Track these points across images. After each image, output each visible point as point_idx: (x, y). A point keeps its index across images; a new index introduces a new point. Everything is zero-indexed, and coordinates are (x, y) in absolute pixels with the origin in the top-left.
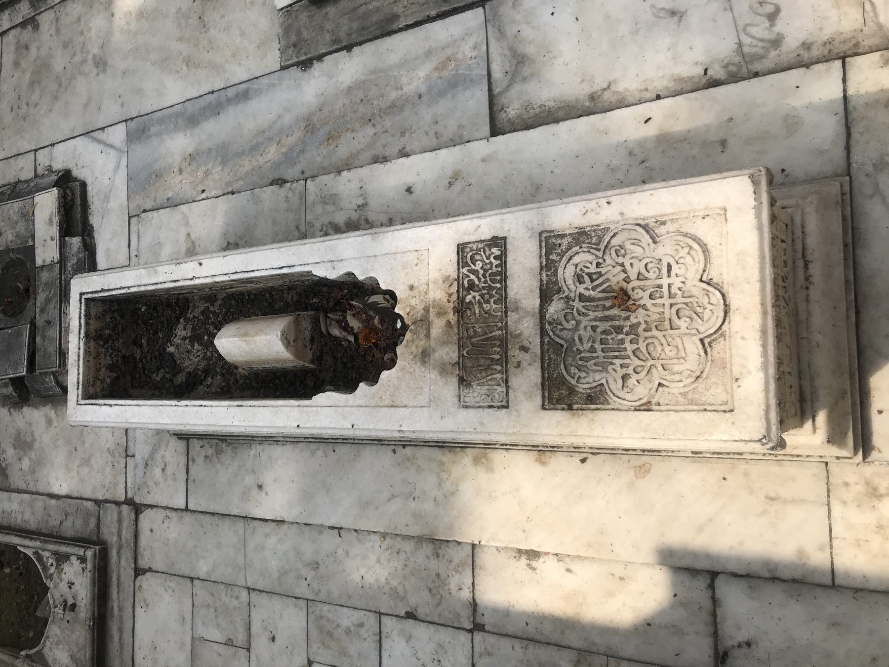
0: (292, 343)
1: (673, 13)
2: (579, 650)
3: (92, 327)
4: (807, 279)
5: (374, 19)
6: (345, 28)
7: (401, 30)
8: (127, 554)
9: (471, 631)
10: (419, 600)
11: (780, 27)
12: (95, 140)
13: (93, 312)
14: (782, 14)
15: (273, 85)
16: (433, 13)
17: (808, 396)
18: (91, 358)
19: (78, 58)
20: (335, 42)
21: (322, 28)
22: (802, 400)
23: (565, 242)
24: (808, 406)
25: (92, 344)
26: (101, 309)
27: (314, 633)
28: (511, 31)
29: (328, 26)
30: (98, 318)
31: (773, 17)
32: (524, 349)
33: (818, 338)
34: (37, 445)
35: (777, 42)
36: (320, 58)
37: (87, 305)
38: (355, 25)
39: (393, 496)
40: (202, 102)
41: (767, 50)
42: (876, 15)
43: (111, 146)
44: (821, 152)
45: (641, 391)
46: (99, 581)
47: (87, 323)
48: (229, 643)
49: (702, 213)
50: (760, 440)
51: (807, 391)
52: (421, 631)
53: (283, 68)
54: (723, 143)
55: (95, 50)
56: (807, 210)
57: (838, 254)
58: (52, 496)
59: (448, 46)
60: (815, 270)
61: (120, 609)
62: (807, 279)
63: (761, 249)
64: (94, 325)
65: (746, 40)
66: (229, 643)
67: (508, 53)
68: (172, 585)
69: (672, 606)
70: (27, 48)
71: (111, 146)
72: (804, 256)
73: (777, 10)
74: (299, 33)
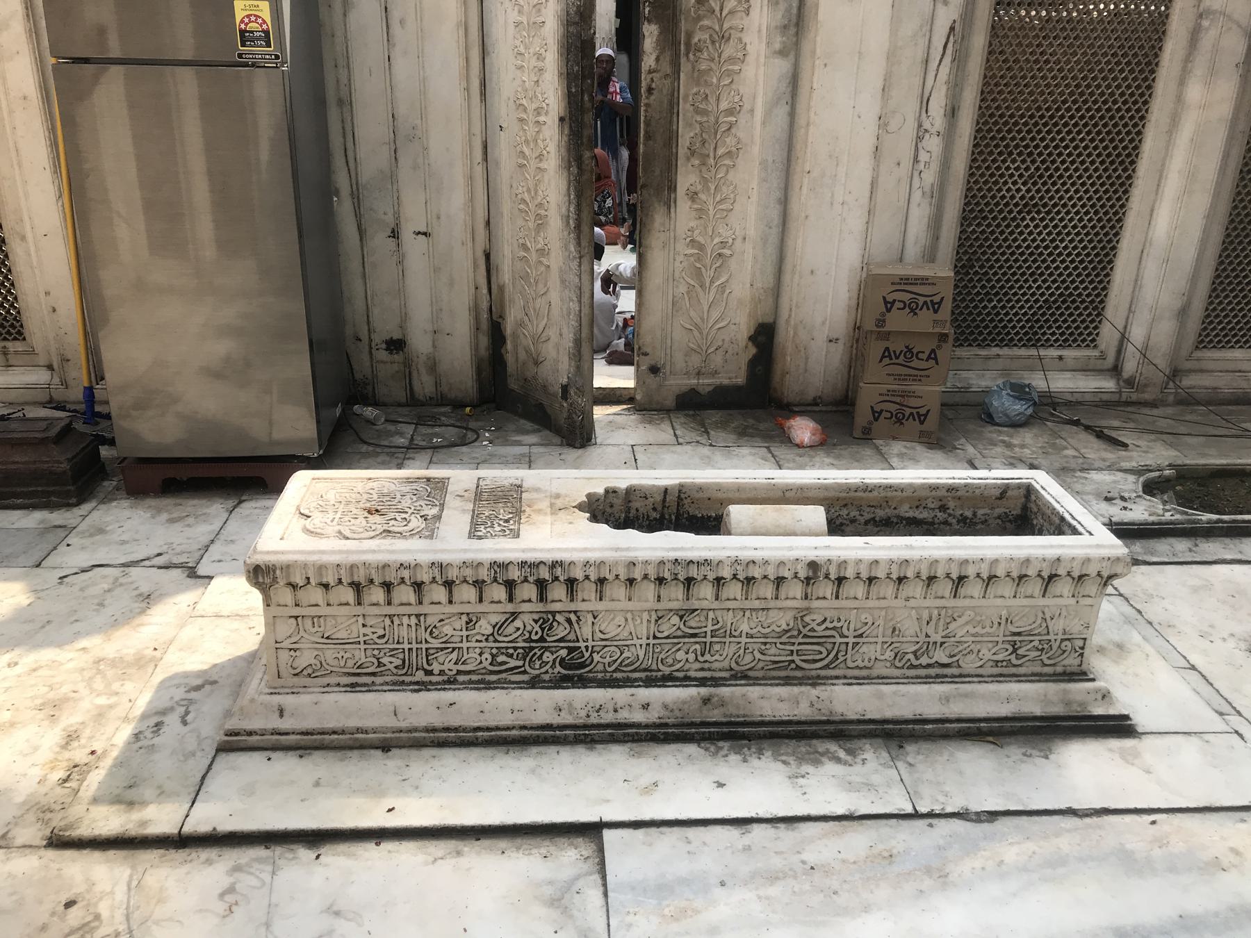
1: (337, 914)
14: (220, 891)
31: (231, 890)
41: (248, 865)
42: (131, 876)
65: (266, 877)
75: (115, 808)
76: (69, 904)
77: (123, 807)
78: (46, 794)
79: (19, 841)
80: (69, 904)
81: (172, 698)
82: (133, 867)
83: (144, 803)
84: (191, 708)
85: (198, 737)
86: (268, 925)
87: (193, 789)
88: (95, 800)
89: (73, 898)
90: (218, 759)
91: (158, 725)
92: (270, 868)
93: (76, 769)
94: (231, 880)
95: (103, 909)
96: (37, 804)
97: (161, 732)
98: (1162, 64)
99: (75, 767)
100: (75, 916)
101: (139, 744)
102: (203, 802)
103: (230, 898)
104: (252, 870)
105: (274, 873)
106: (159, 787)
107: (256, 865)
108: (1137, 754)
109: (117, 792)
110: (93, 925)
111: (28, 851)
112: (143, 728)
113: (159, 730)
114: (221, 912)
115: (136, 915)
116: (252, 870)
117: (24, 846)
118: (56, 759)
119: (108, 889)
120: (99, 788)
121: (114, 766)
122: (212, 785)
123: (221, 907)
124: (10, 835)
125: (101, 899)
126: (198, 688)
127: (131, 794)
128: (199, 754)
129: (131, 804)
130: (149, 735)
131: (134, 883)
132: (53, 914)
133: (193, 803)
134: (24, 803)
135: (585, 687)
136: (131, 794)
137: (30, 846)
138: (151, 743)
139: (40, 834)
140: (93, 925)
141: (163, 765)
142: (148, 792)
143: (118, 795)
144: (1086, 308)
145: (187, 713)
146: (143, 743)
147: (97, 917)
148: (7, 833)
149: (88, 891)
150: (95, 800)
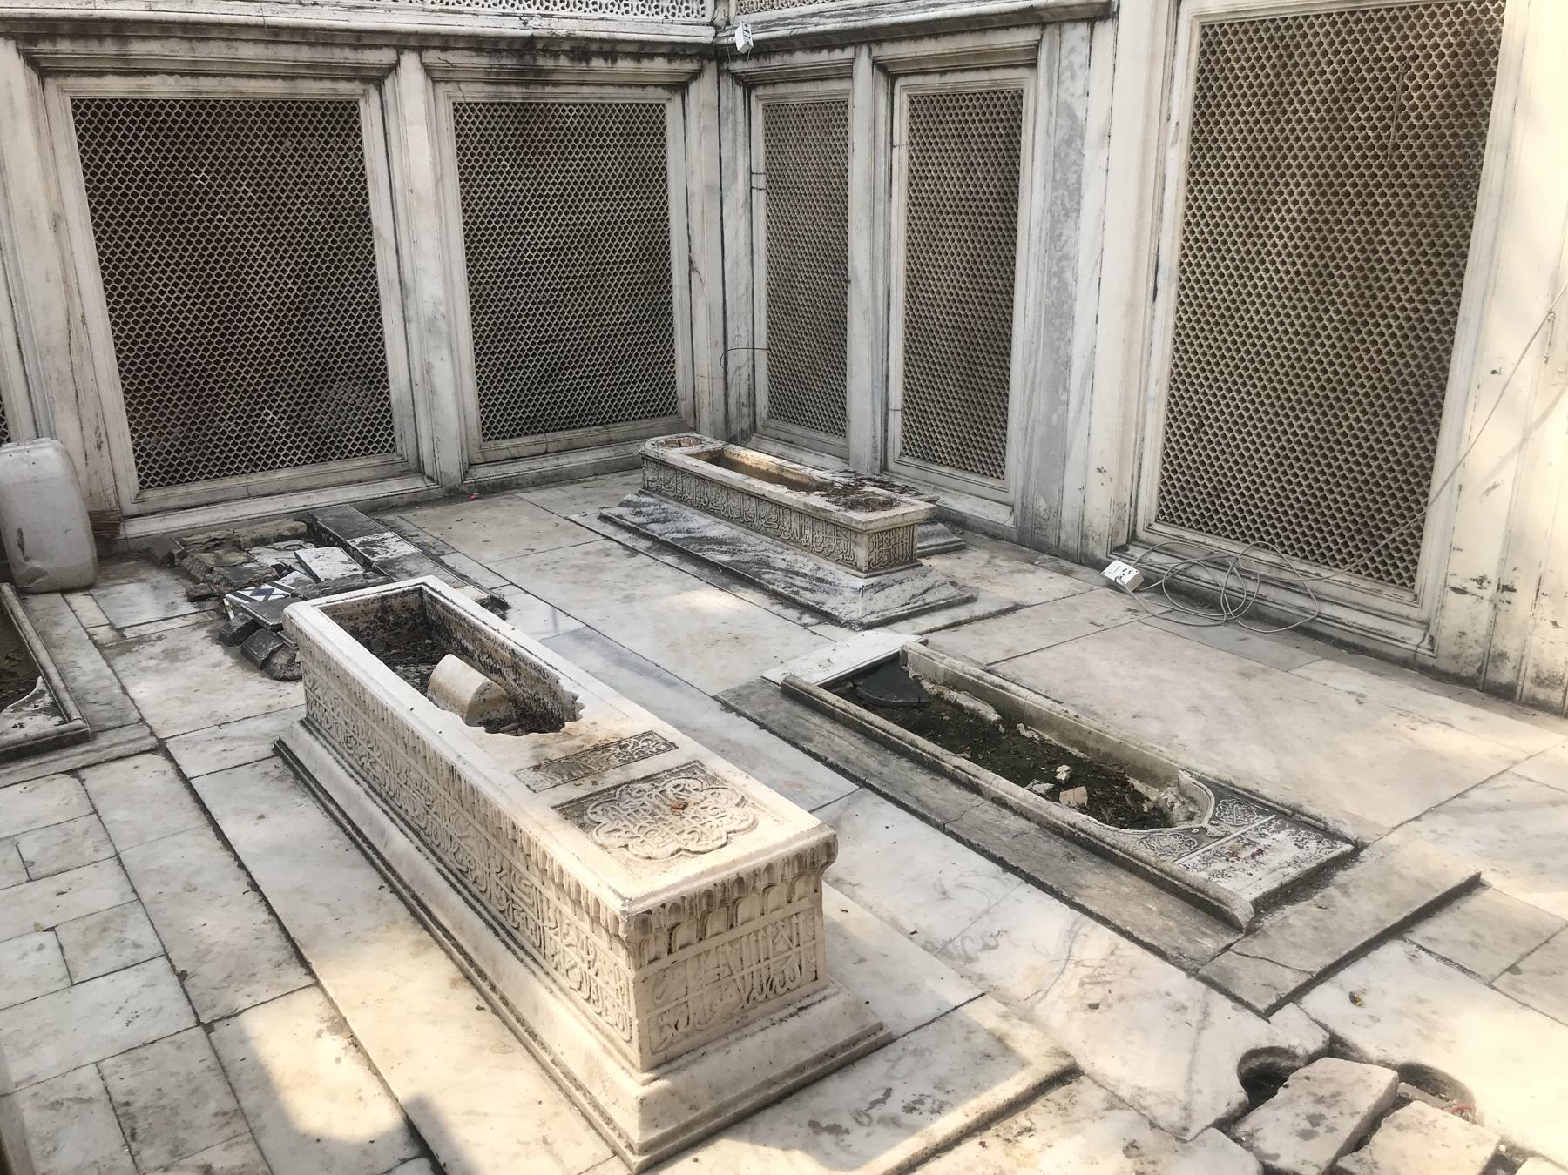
0: (483, 698)
1: (944, 893)
2: (241, 1108)
3: (393, 601)
4: (781, 1020)
5: (798, 730)
6: (777, 717)
7: (803, 749)
8: (92, 758)
9: (199, 1023)
10: (209, 973)
11: (982, 955)
12: (554, 615)
13: (409, 598)
14: (993, 952)
15: (694, 697)
16: (830, 759)
17: (675, 1065)
18: (362, 608)
19: (623, 585)
20: (761, 716)
21: (767, 704)
22: (668, 1061)
23: (699, 774)
24: (666, 1068)
25: (377, 605)
26: (413, 606)
27: (96, 919)
28: (853, 810)
29: (770, 708)
30: (403, 605)
31: (987, 947)
32: (595, 783)
33: (735, 1050)
34: (177, 665)
35: (969, 960)
36: (740, 714)
37: (414, 591)
38: (784, 721)
39: (328, 905)
40: (644, 663)
41: (960, 957)
42: (1039, 1002)
43: (556, 625)
44: (901, 1016)
45: (613, 840)
46: (42, 743)
47: (396, 595)
48: (27, 865)
49: (776, 817)
50: (624, 899)
51: (681, 1062)
52: (170, 987)
53: (715, 698)
54: (862, 960)
55: (638, 592)
56: (841, 995)
57: (820, 1046)
58: (123, 688)
59: (811, 781)
60: (794, 1023)
61: (10, 774)
62: (781, 1020)
63: (777, 847)
64: (396, 603)
65: (958, 942)
66: (27, 865)
67: (834, 817)
68: (75, 801)
69: (356, 1147)
70: (608, 555)
71: (556, 625)
72: (800, 1009)
73: (994, 948)
74: (752, 694)
75: (1013, 1045)
76: (1094, 1006)
77: (1008, 1042)
78: (1053, 1127)
79: (1102, 1093)
80: (1094, 1006)
81: (868, 1135)
82: (1032, 1008)
83: (991, 1033)
84: (865, 1106)
85: (893, 1067)
86: (987, 911)
87: (946, 1019)
88: (1024, 1064)
89: (1089, 1011)
90: (900, 1034)
91: (910, 1109)
92: (950, 946)
93: (1009, 1137)
94: (979, 954)
95: (1074, 988)
96: (1066, 1122)
97: (916, 1098)
98: (381, 295)
99: (1009, 1141)
100: (1096, 995)
101: (944, 1097)
102: (947, 1002)
103: (992, 942)
104: (961, 952)
105: (951, 941)
106: (967, 1039)
107: (955, 953)
108: (43, 1140)
109: (1001, 1059)
110: (1088, 980)
111: (1099, 1078)
112: (926, 1114)
113: (915, 1102)
114: (1005, 935)
115: (1056, 969)
116: (961, 952)
117: (1100, 1086)
118: (1019, 1165)
119: (1061, 1001)
120: (1013, 1074)
121: (984, 1089)
122: (930, 1011)
123: (1002, 940)
124: (1107, 1105)
125: (1071, 997)
126: (835, 1129)
127: (993, 1049)
128: (911, 1047)
129: (1000, 1040)
130: (928, 1101)
131: (1041, 994)
132: (1110, 1006)
133: (956, 1007)
134: (1077, 1132)
135: (1072, 298)
136: (993, 1049)
137: (1095, 1082)
138: (936, 1092)
139: (1081, 1088)
140: (1088, 980)
141: (946, 1058)
142: (980, 1040)
143: (1003, 1055)
144: (562, 402)
145: (874, 1104)
146: (940, 1096)
147: (1082, 984)
148: (1107, 1109)
149: (1074, 1009)
150: (1024, 1064)
